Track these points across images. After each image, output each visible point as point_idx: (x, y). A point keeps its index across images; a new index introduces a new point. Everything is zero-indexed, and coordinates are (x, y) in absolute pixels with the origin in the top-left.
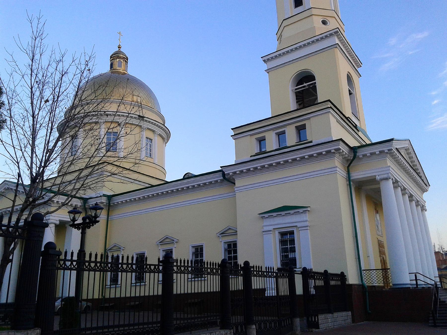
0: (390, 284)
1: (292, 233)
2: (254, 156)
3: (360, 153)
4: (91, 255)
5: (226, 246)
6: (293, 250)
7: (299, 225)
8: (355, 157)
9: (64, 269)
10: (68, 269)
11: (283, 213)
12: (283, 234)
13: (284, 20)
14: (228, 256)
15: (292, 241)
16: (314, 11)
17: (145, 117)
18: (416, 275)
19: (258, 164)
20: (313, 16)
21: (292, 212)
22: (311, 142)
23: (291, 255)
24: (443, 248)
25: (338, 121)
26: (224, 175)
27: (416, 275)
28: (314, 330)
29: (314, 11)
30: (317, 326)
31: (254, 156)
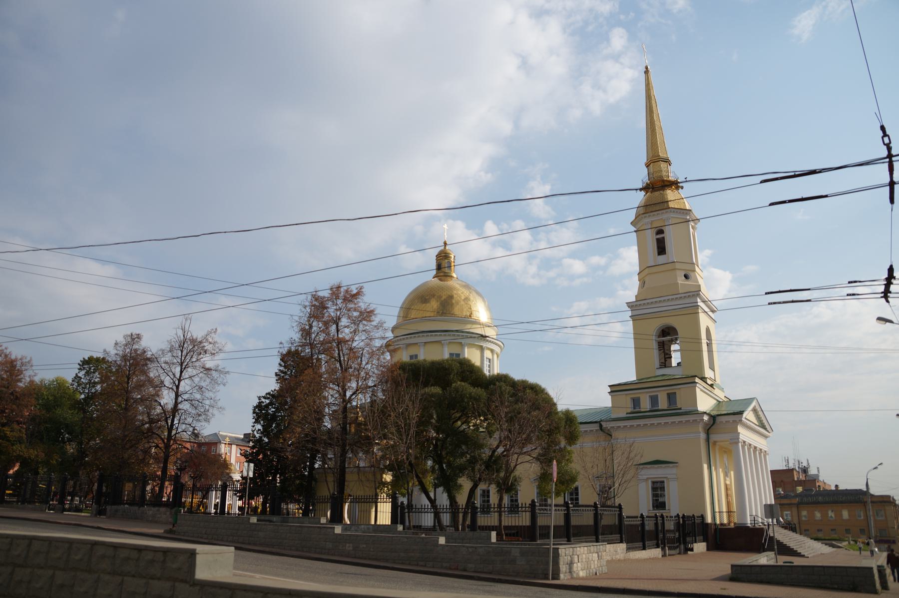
0: (669, 531)
1: (663, 482)
2: (630, 413)
3: (719, 419)
4: (522, 504)
5: (482, 491)
6: (663, 496)
7: (669, 476)
8: (714, 423)
9: (443, 513)
10: (445, 512)
11: (656, 466)
12: (653, 483)
13: (648, 267)
14: (870, 569)
15: (663, 489)
16: (678, 266)
17: (488, 337)
18: (754, 517)
19: (628, 423)
20: (677, 270)
21: (663, 465)
22: (680, 409)
23: (661, 500)
24: (594, 576)
25: (701, 390)
26: (601, 426)
27: (754, 517)
28: (689, 552)
29: (678, 266)
30: (692, 550)
31: (630, 413)
